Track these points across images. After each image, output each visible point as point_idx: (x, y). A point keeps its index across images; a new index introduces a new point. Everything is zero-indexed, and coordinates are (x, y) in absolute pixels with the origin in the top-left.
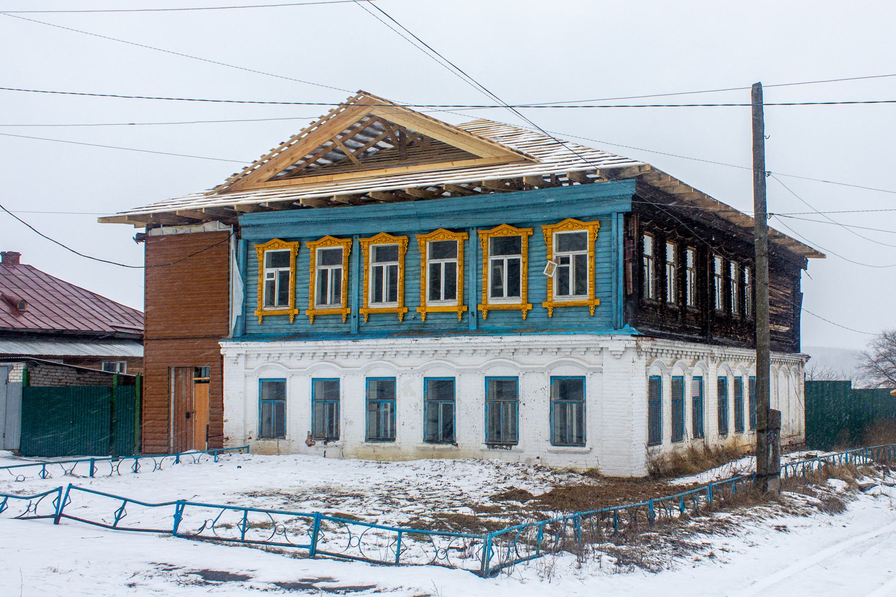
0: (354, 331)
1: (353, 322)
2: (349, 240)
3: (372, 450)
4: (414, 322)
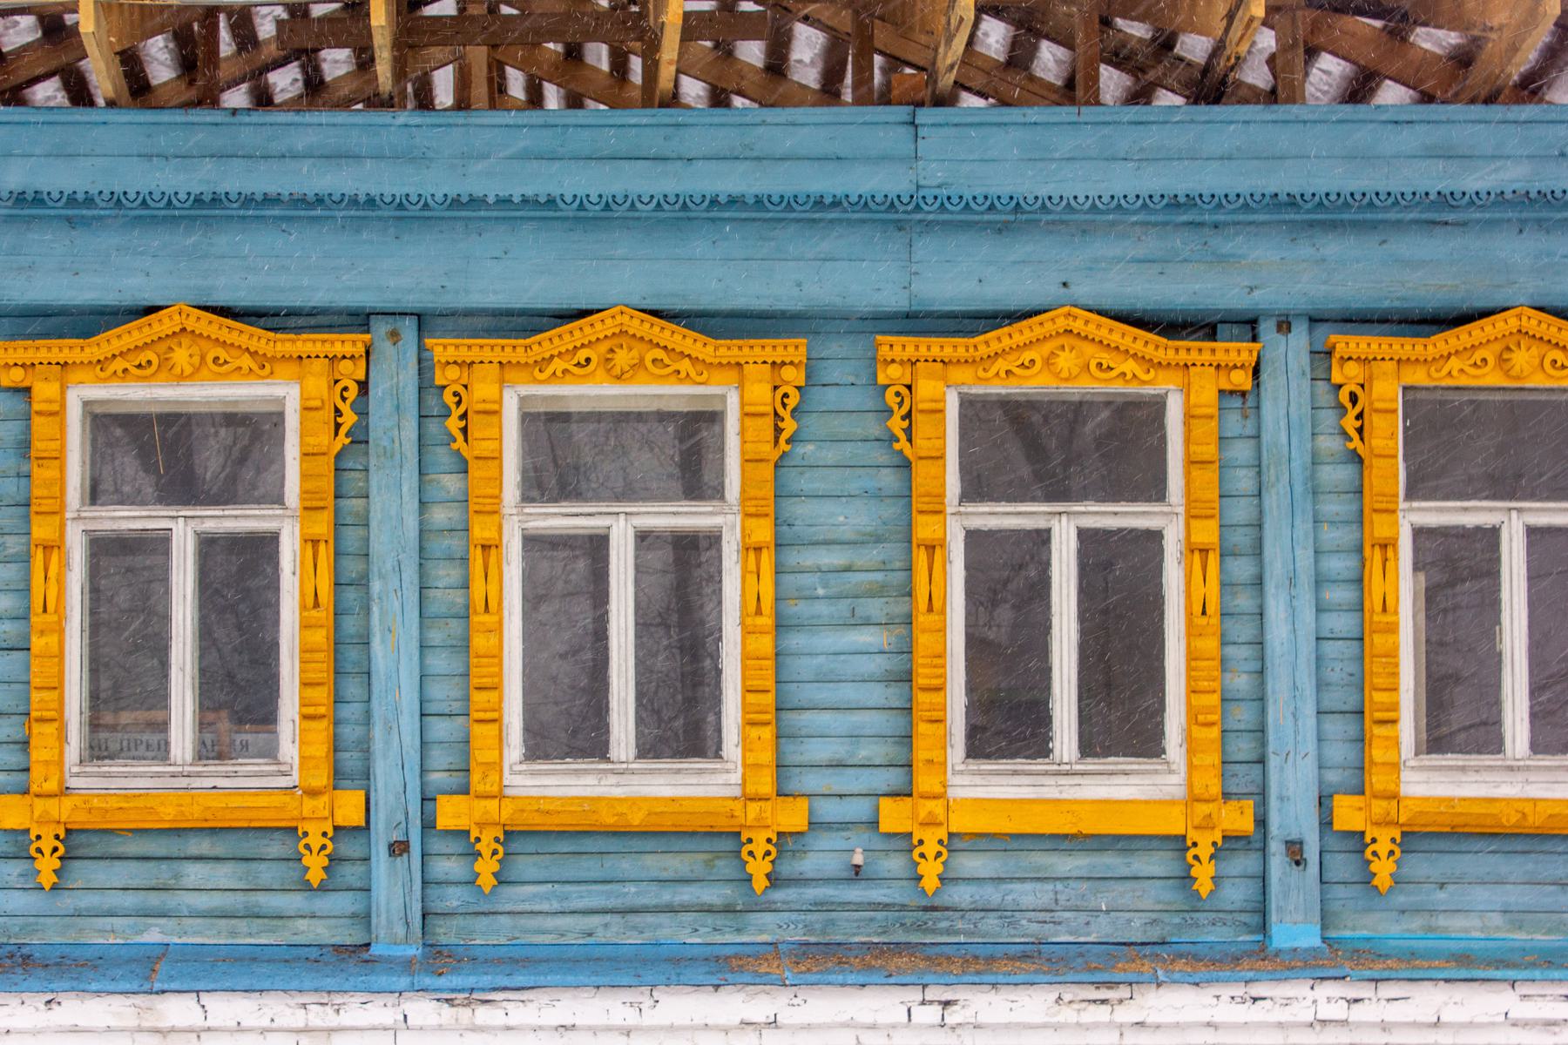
0: (393, 933)
1: (392, 888)
2: (349, 344)
4: (854, 893)
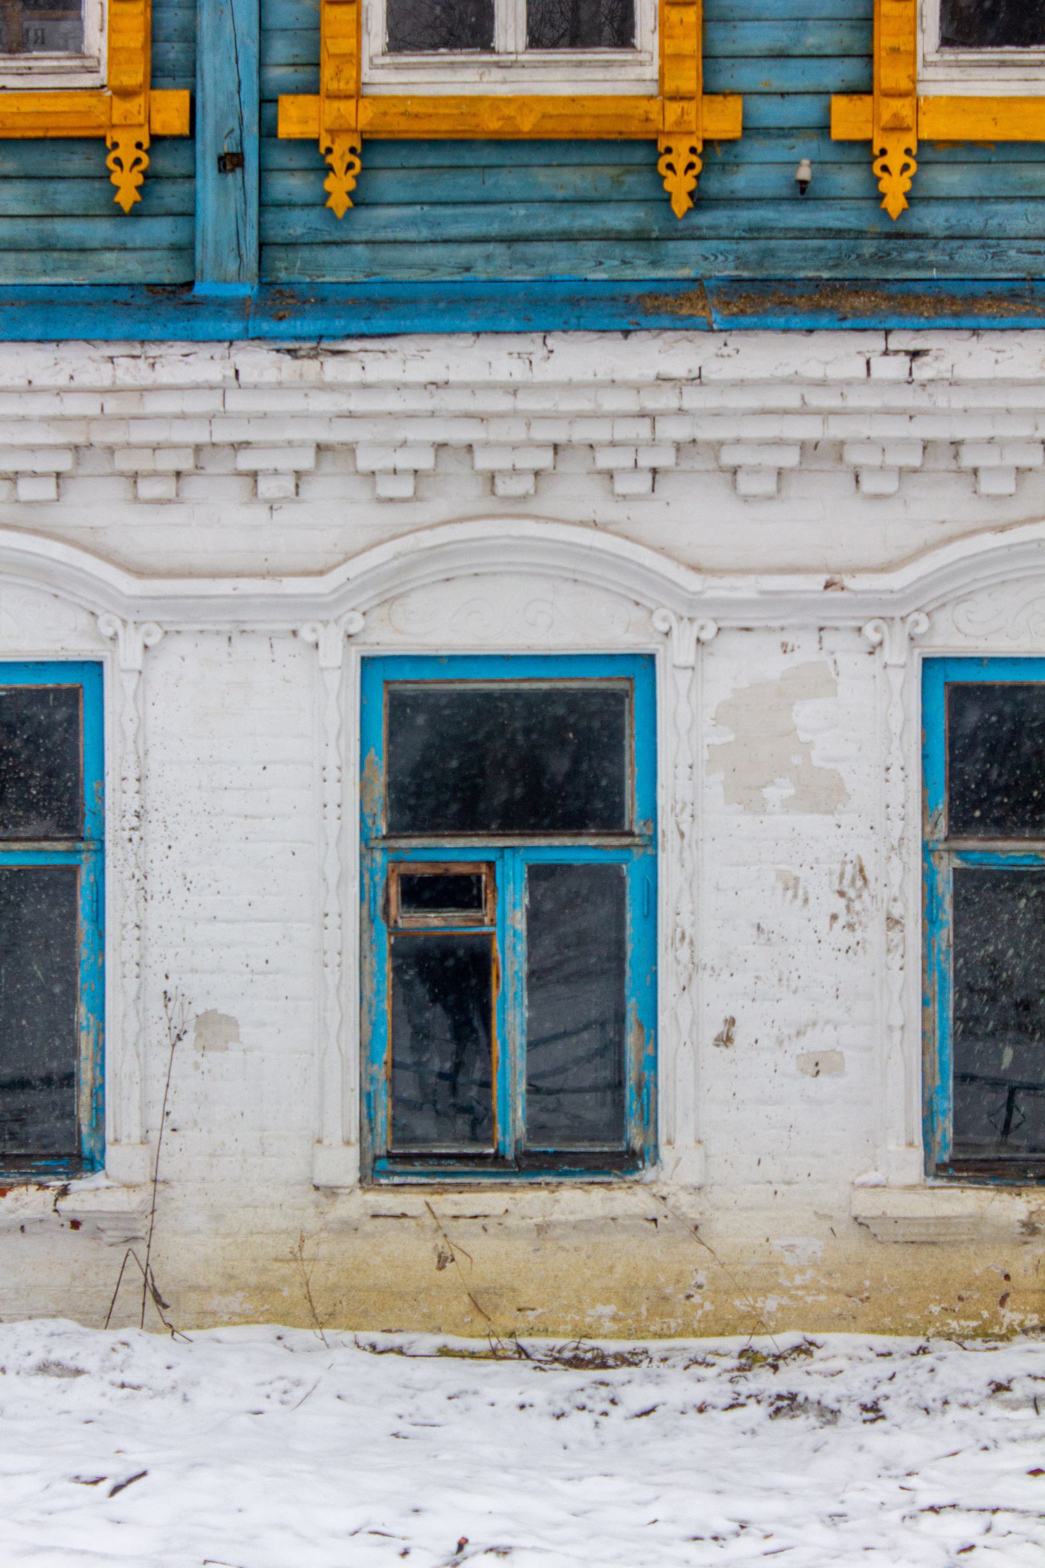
1: (220, 207)
3: (421, 1252)
4: (799, 217)
